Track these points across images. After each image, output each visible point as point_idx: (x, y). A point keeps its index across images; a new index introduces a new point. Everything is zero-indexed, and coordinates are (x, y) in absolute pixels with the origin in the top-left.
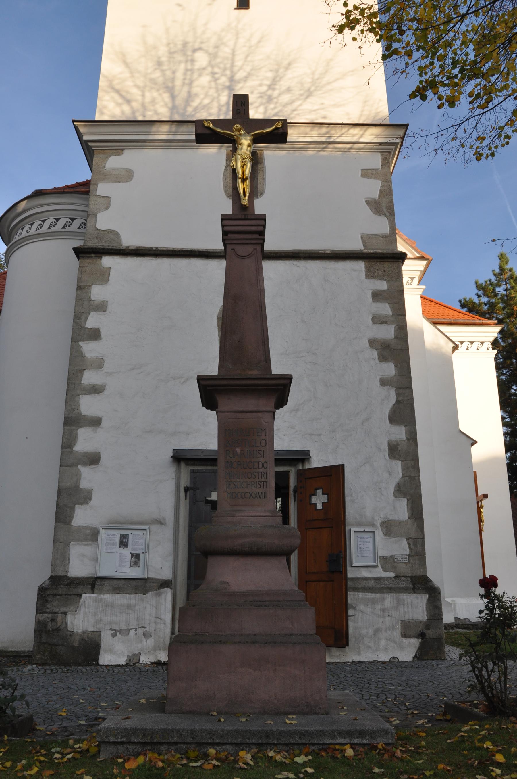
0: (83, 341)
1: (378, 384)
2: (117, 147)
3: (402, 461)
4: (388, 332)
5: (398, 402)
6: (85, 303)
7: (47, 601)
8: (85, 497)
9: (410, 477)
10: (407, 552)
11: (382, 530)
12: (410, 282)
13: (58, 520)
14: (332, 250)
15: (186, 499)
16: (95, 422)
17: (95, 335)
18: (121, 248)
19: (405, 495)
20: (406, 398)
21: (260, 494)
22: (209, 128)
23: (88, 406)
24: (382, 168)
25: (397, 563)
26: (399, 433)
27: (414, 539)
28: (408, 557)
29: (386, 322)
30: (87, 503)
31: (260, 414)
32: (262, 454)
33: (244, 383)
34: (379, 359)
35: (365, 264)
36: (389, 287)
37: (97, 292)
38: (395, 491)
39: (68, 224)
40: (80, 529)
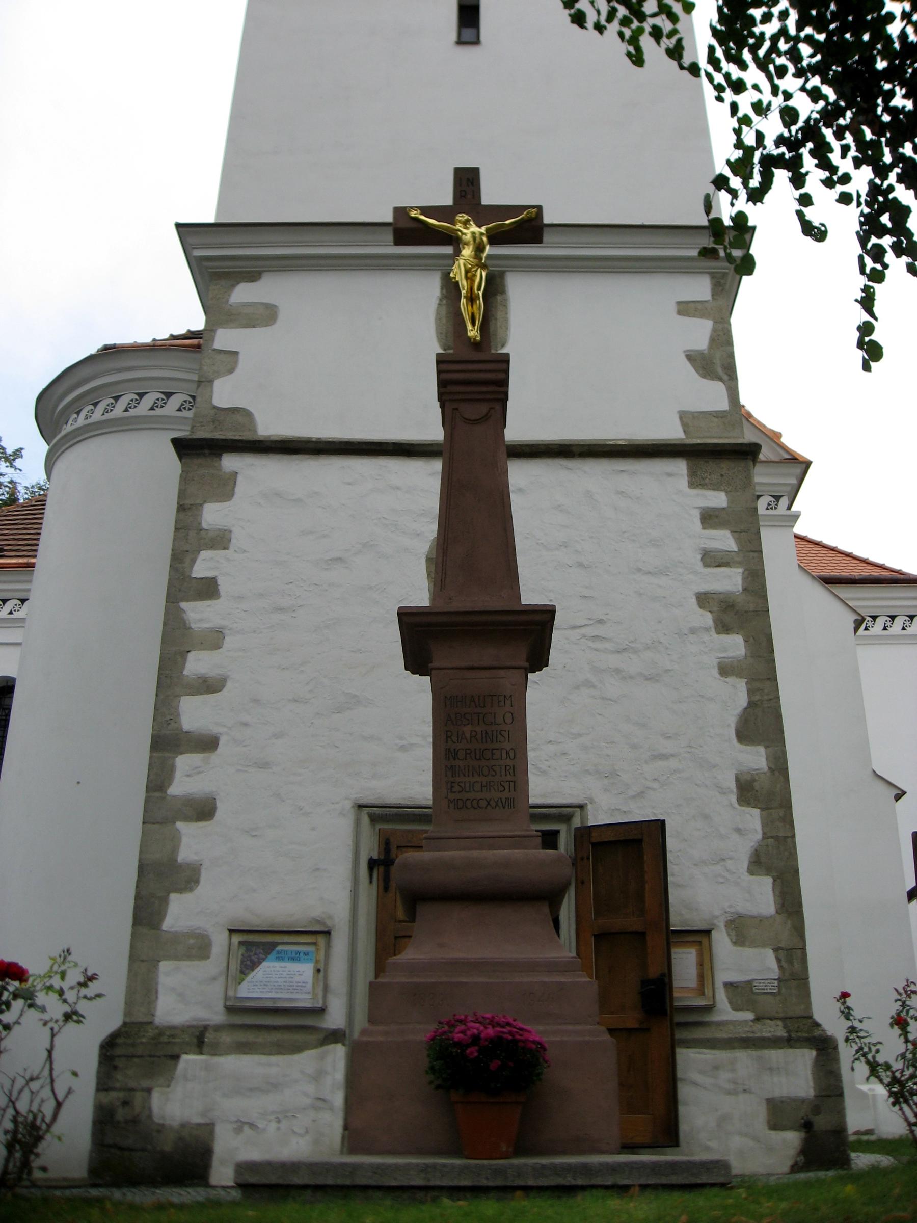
0: (188, 601)
1: (715, 672)
2: (251, 272)
3: (762, 809)
4: (730, 581)
5: (751, 704)
6: (192, 534)
7: (115, 1068)
8: (187, 878)
9: (776, 838)
10: (775, 973)
11: (729, 935)
12: (773, 505)
13: (137, 921)
14: (629, 440)
15: (371, 882)
16: (207, 744)
17: (208, 589)
18: (255, 438)
19: (768, 871)
20: (766, 697)
21: (504, 801)
22: (416, 219)
23: (194, 714)
24: (713, 299)
25: (757, 994)
26: (756, 758)
27: (787, 950)
28: (776, 983)
29: (727, 564)
30: (191, 890)
31: (502, 673)
32: (507, 736)
33: (476, 638)
34: (716, 628)
35: (688, 464)
36: (730, 502)
37: (213, 515)
38: (750, 862)
39: (160, 403)
40: (176, 938)
